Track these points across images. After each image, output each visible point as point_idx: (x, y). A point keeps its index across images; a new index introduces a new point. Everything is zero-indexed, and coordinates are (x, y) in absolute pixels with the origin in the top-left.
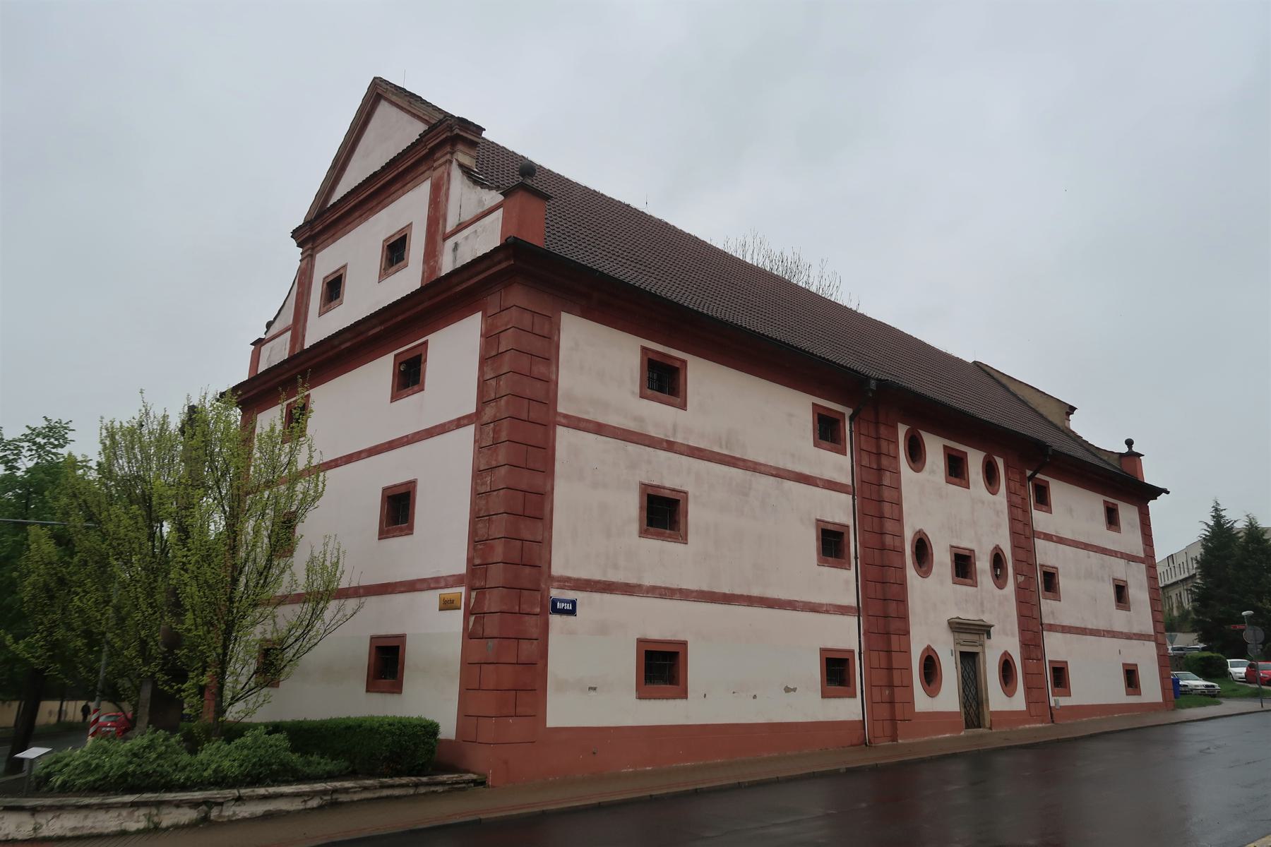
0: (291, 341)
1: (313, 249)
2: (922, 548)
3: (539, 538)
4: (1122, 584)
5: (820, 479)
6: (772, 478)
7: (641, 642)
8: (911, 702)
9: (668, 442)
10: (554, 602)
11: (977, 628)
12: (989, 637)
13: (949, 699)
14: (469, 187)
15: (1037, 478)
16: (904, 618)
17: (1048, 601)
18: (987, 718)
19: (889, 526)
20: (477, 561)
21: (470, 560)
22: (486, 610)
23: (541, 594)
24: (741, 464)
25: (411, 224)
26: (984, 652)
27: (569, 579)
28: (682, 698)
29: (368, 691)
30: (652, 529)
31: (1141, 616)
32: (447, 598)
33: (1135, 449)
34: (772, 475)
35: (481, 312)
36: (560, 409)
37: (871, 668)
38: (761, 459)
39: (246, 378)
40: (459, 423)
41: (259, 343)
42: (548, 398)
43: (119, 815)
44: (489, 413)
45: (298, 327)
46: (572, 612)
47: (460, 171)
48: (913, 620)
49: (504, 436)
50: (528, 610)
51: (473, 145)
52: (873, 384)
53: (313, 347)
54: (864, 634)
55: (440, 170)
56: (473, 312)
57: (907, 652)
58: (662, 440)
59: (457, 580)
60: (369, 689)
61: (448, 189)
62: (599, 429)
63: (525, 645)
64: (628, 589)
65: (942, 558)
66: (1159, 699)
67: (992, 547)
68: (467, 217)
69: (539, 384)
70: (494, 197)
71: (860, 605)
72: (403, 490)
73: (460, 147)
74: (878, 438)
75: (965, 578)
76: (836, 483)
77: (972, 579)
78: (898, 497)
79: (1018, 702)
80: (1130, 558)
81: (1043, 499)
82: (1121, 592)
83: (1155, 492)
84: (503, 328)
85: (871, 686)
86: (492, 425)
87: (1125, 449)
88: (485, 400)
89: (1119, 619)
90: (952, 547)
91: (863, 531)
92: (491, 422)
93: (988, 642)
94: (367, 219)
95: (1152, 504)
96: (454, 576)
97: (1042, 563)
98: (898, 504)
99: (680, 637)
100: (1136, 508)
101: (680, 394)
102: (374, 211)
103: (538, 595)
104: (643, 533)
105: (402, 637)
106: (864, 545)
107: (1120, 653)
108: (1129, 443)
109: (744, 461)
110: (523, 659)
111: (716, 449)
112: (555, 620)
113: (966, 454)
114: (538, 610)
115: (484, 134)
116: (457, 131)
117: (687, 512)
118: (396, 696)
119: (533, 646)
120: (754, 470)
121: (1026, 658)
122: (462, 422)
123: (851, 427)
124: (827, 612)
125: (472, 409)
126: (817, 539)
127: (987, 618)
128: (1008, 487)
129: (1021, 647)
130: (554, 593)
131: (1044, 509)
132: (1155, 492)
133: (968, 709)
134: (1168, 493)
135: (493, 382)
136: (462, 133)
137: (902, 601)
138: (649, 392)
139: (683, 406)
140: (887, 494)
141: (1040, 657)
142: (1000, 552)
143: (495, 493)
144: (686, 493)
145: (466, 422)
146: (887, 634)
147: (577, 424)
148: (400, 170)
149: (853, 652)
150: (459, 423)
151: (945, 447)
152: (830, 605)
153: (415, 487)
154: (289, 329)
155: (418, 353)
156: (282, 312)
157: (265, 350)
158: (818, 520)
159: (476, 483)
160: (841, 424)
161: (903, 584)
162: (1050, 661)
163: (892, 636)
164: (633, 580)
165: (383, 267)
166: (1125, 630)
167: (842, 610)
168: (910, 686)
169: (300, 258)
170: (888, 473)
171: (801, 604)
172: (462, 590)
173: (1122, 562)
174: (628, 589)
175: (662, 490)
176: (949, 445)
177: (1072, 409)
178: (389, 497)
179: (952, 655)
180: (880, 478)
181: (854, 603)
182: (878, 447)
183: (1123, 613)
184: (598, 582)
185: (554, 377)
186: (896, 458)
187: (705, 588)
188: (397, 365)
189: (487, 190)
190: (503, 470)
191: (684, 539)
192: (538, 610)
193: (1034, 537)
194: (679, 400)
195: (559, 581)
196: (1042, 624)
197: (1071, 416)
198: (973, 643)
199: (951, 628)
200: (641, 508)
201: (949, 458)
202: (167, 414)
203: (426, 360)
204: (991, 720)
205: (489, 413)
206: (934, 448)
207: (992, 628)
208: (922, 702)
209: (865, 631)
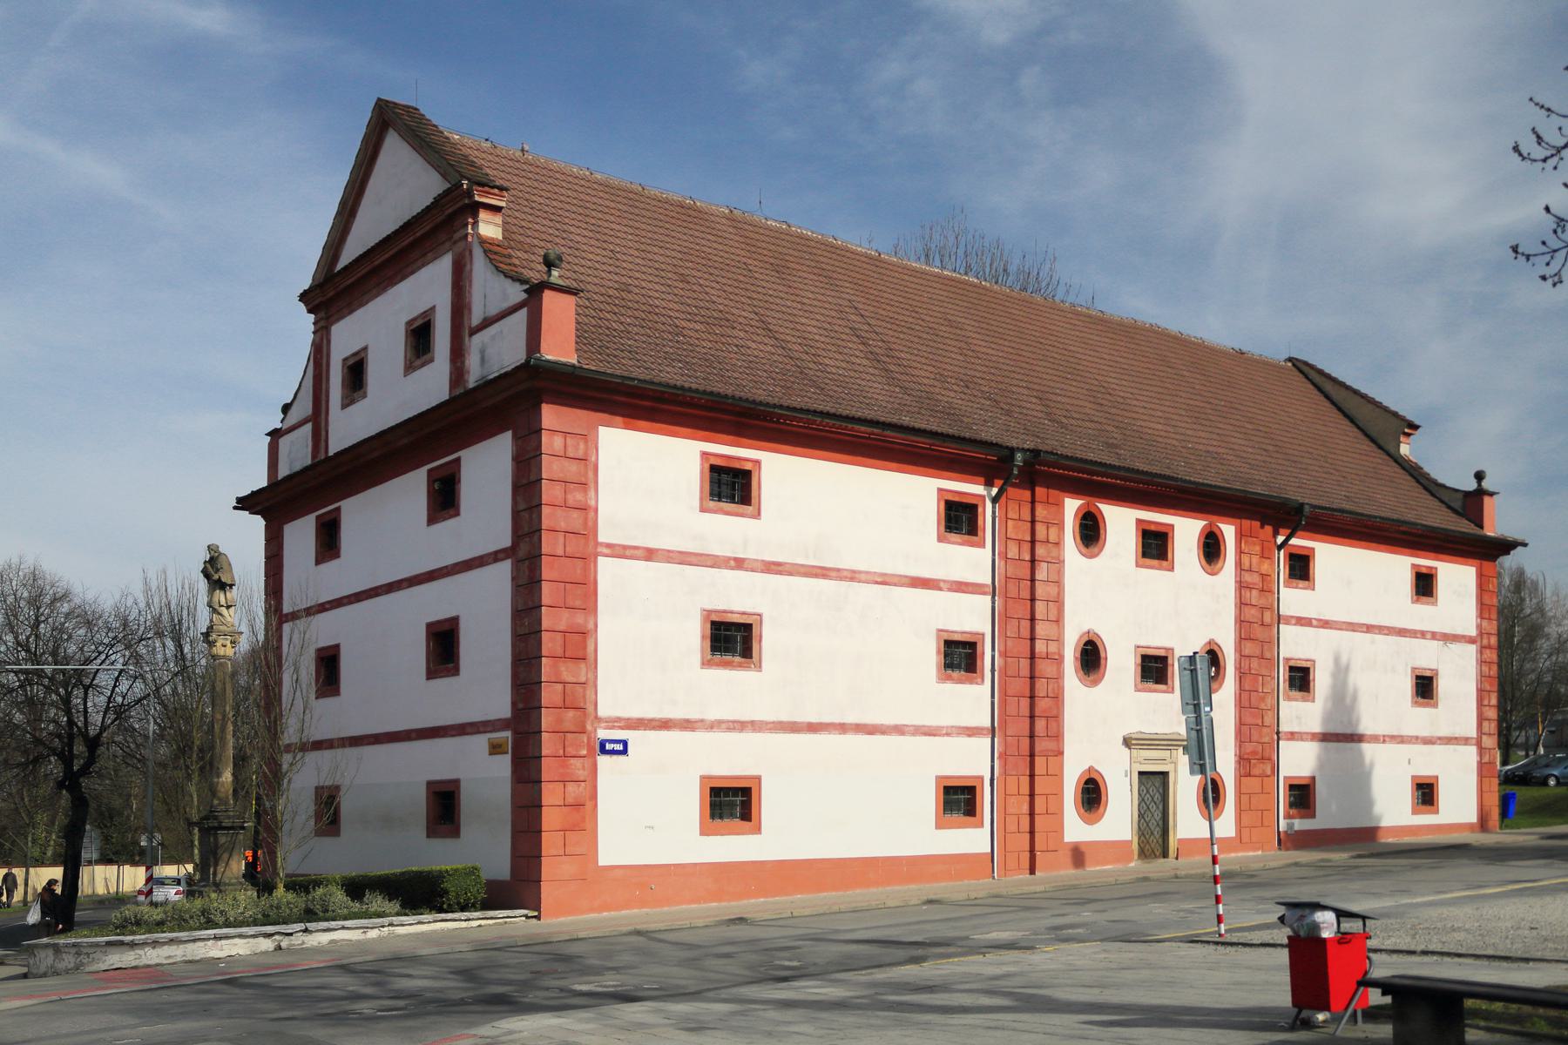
0: (313, 437)
3: (583, 679)
5: (944, 581)
9: (736, 559)
10: (603, 744)
14: (492, 273)
15: (1293, 546)
17: (1294, 703)
20: (521, 706)
21: (514, 704)
24: (834, 574)
25: (434, 307)
26: (1176, 771)
27: (619, 719)
28: (757, 834)
29: (428, 836)
30: (718, 657)
33: (1486, 484)
34: (877, 583)
35: (510, 432)
36: (601, 539)
39: (266, 485)
40: (496, 557)
41: (275, 435)
45: (318, 419)
46: (624, 752)
50: (574, 753)
53: (338, 454)
54: (1000, 757)
56: (502, 430)
57: (1058, 776)
58: (729, 559)
63: (571, 787)
64: (687, 725)
65: (1121, 663)
68: (493, 311)
69: (575, 514)
71: (996, 725)
72: (446, 627)
76: (967, 584)
78: (1059, 594)
81: (1301, 568)
82: (1425, 687)
86: (527, 562)
88: (520, 533)
94: (384, 290)
97: (1288, 656)
101: (753, 501)
102: (393, 280)
105: (456, 782)
107: (1409, 763)
108: (1479, 476)
109: (838, 570)
110: (570, 800)
112: (604, 761)
114: (584, 752)
118: (337, 838)
119: (581, 789)
120: (852, 579)
123: (994, 512)
125: (507, 542)
126: (938, 652)
128: (1239, 564)
130: (603, 734)
131: (1300, 586)
133: (1147, 837)
138: (712, 504)
141: (1269, 773)
142: (1216, 648)
147: (621, 552)
148: (418, 234)
149: (981, 778)
150: (496, 557)
152: (952, 727)
153: (458, 624)
154: (310, 421)
156: (299, 395)
157: (284, 442)
159: (516, 624)
165: (408, 358)
169: (313, 330)
171: (911, 728)
172: (508, 734)
173: (1435, 645)
174: (687, 725)
175: (729, 615)
179: (1126, 776)
184: (651, 720)
187: (775, 719)
193: (1279, 623)
194: (751, 508)
196: (1278, 733)
200: (703, 637)
203: (459, 481)
204: (1178, 849)
206: (1121, 521)
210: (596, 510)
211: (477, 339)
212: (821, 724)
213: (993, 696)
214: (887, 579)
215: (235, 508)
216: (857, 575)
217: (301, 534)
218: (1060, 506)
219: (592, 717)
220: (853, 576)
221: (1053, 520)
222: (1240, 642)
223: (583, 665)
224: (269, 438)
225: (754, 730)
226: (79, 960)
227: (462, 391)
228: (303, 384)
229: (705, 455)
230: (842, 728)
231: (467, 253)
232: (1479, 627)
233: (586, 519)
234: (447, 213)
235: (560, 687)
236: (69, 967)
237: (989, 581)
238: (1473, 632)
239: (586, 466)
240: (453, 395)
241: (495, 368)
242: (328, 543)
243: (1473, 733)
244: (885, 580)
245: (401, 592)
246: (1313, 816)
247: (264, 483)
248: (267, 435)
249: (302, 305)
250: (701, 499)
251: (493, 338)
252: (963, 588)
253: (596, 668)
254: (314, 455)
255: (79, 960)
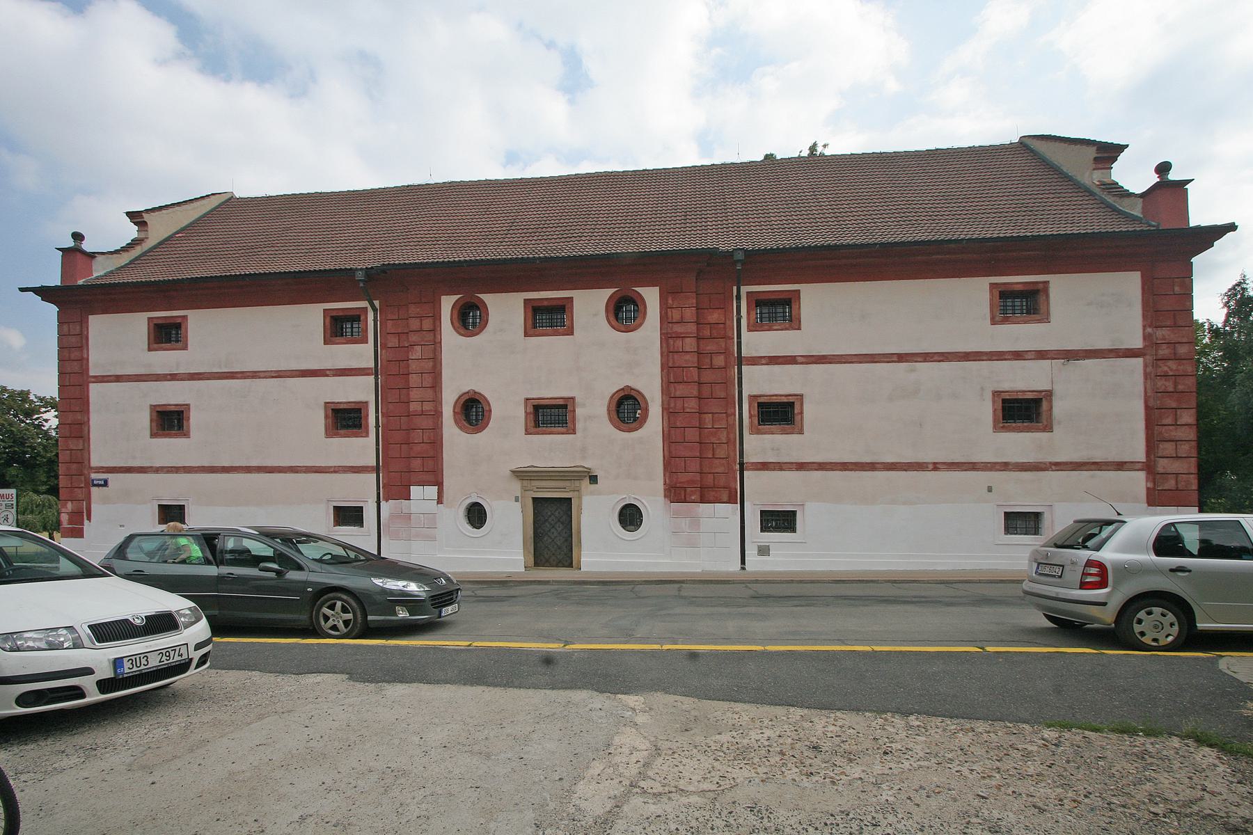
10: (93, 480)
11: (562, 474)
23: (85, 478)
24: (239, 375)
34: (273, 377)
64: (142, 470)
103: (83, 478)
108: (1163, 168)
112: (94, 490)
128: (664, 319)
130: (93, 476)
138: (156, 346)
174: (142, 470)
200: (151, 421)
202: (1052, 545)
210: (88, 359)
212: (232, 467)
214: (281, 374)
216: (257, 374)
219: (87, 467)
220: (254, 375)
221: (684, 305)
222: (668, 386)
223: (81, 441)
225: (185, 472)
229: (993, 286)
230: (248, 470)
232: (1146, 337)
233: (82, 366)
238: (1138, 343)
239: (82, 337)
243: (1140, 456)
244: (279, 375)
252: (347, 372)
253: (89, 441)
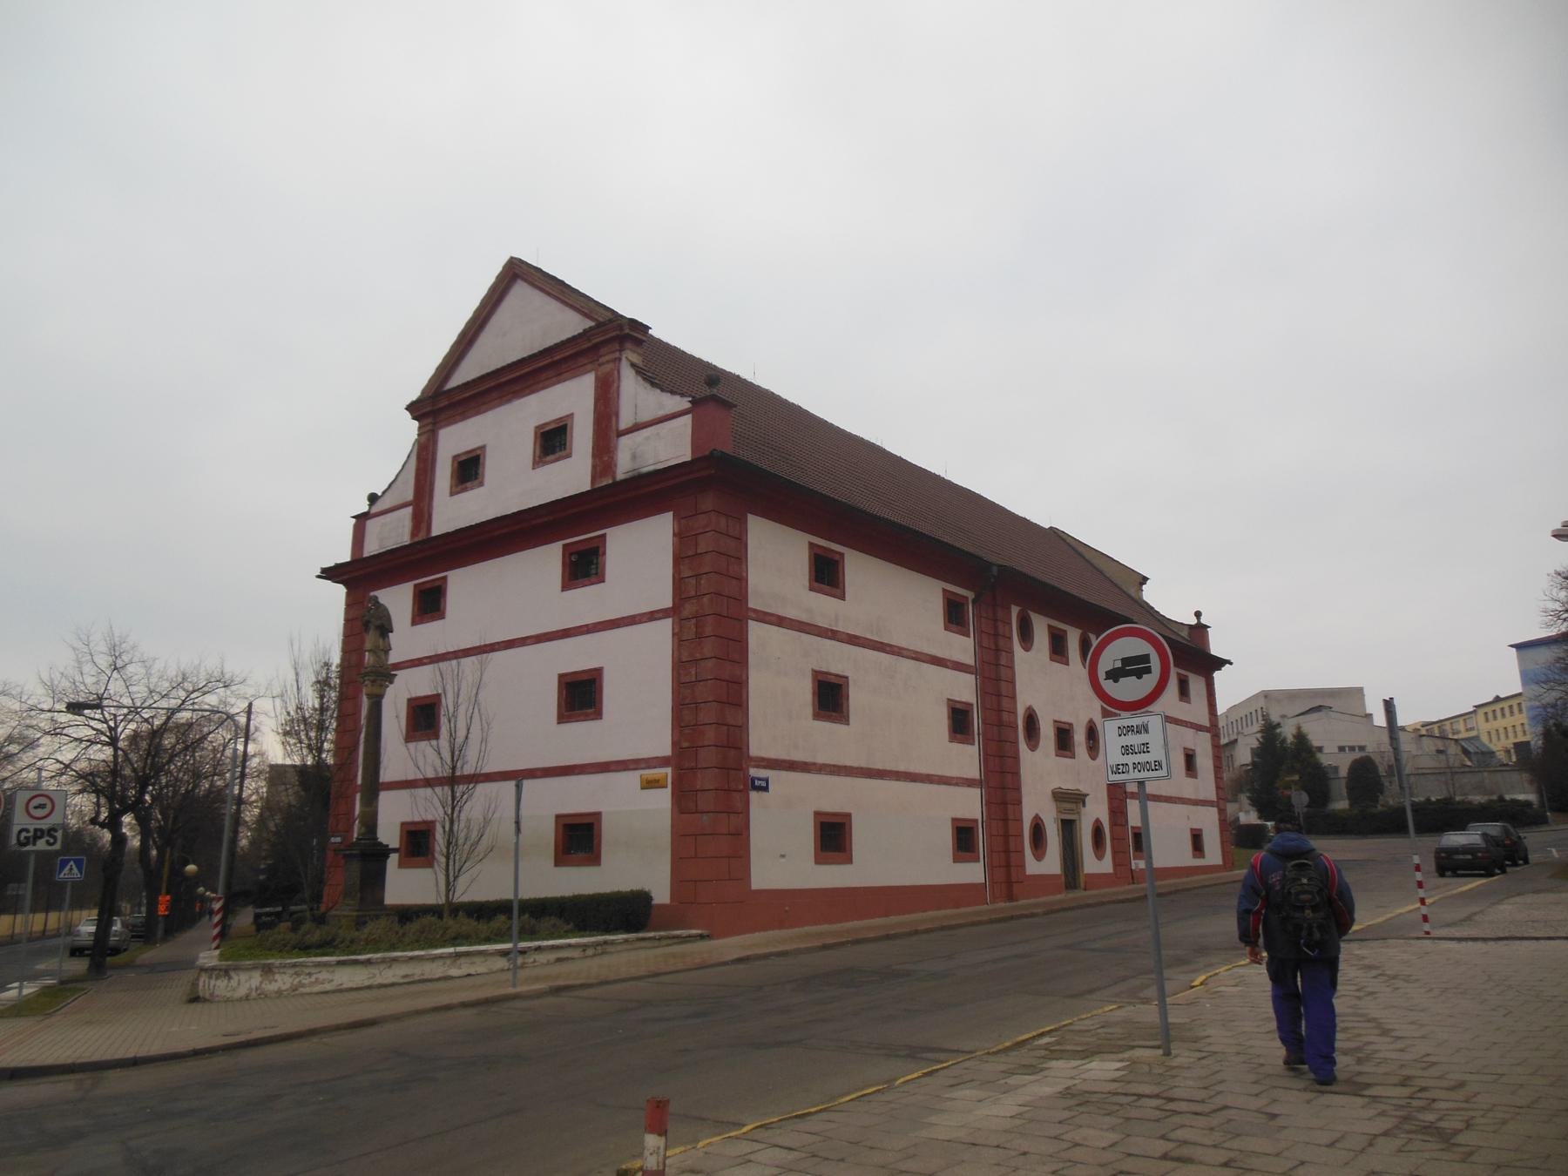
1: (434, 424)
2: (1031, 721)
3: (740, 724)
4: (1191, 753)
5: (949, 661)
6: (913, 662)
7: (817, 814)
8: (1022, 866)
10: (753, 780)
11: (1072, 796)
12: (1084, 805)
13: (1051, 863)
14: (645, 388)
16: (1018, 789)
18: (1082, 880)
19: (1005, 703)
20: (685, 745)
21: (674, 744)
22: (698, 787)
24: (888, 649)
27: (763, 759)
31: (1205, 786)
32: (650, 778)
33: (1204, 621)
36: (751, 605)
37: (991, 835)
38: (903, 644)
40: (652, 616)
42: (740, 595)
43: (444, 964)
44: (689, 610)
46: (766, 789)
47: (634, 372)
48: (1025, 790)
49: (708, 630)
51: (638, 343)
52: (995, 569)
54: (986, 805)
55: (607, 368)
57: (1020, 820)
59: (662, 762)
60: (558, 862)
61: (618, 387)
62: (780, 622)
65: (1047, 732)
66: (1219, 862)
67: (1087, 720)
68: (645, 417)
70: (683, 403)
73: (628, 345)
74: (995, 620)
75: (1065, 750)
77: (1070, 751)
79: (1106, 866)
80: (1198, 728)
82: (1190, 759)
83: (1220, 663)
84: (701, 531)
85: (991, 851)
86: (694, 621)
87: (1193, 621)
89: (1188, 788)
90: (1055, 721)
91: (984, 708)
92: (693, 618)
93: (1083, 810)
94: (509, 401)
95: (1217, 675)
96: (657, 757)
98: (1012, 682)
99: (846, 810)
100: (1204, 679)
103: (741, 773)
104: (817, 716)
106: (984, 723)
108: (1198, 614)
111: (869, 636)
112: (753, 795)
113: (1065, 632)
114: (742, 787)
115: (650, 331)
116: (627, 331)
117: (848, 696)
121: (1113, 824)
122: (657, 616)
123: (973, 610)
124: (957, 784)
127: (1083, 789)
129: (1110, 814)
130: (753, 772)
132: (1220, 663)
134: (1231, 664)
135: (693, 581)
136: (631, 333)
137: (1016, 774)
138: (816, 584)
139: (843, 598)
140: (1004, 672)
143: (701, 683)
144: (847, 678)
145: (660, 615)
146: (1005, 803)
147: (765, 618)
149: (976, 821)
150: (652, 616)
151: (1050, 627)
155: (595, 545)
157: (371, 525)
158: (949, 699)
160: (966, 607)
161: (1016, 758)
162: (1132, 827)
163: (1009, 806)
164: (809, 759)
166: (1193, 797)
167: (969, 783)
168: (1022, 852)
170: (1004, 653)
171: (936, 778)
172: (669, 770)
173: (1191, 731)
176: (825, 545)
177: (1145, 580)
178: (567, 684)
180: (997, 658)
181: (978, 777)
182: (996, 628)
183: (1190, 780)
185: (745, 574)
186: (1010, 638)
188: (567, 556)
189: (659, 391)
190: (710, 664)
191: (847, 722)
192: (742, 787)
194: (838, 590)
195: (755, 761)
196: (1125, 792)
197: (1144, 586)
198: (1071, 811)
199: (1054, 797)
201: (948, 602)
203: (604, 553)
205: (689, 610)
207: (1088, 797)
208: (1033, 867)
209: (986, 801)
211: (624, 442)
213: (980, 755)
215: (319, 577)
217: (398, 600)
218: (1009, 609)
224: (354, 520)
226: (298, 980)
227: (610, 482)
228: (400, 478)
231: (616, 372)
234: (594, 341)
235: (726, 727)
236: (284, 988)
237: (973, 664)
240: (597, 486)
241: (651, 462)
242: (430, 605)
245: (525, 648)
246: (1439, 851)
247: (348, 559)
248: (353, 517)
249: (408, 413)
250: (810, 580)
251: (647, 438)
254: (414, 533)
255: (298, 980)
